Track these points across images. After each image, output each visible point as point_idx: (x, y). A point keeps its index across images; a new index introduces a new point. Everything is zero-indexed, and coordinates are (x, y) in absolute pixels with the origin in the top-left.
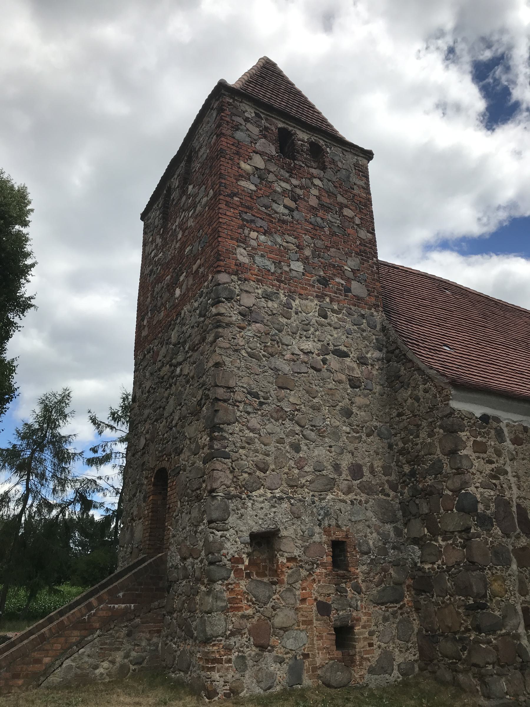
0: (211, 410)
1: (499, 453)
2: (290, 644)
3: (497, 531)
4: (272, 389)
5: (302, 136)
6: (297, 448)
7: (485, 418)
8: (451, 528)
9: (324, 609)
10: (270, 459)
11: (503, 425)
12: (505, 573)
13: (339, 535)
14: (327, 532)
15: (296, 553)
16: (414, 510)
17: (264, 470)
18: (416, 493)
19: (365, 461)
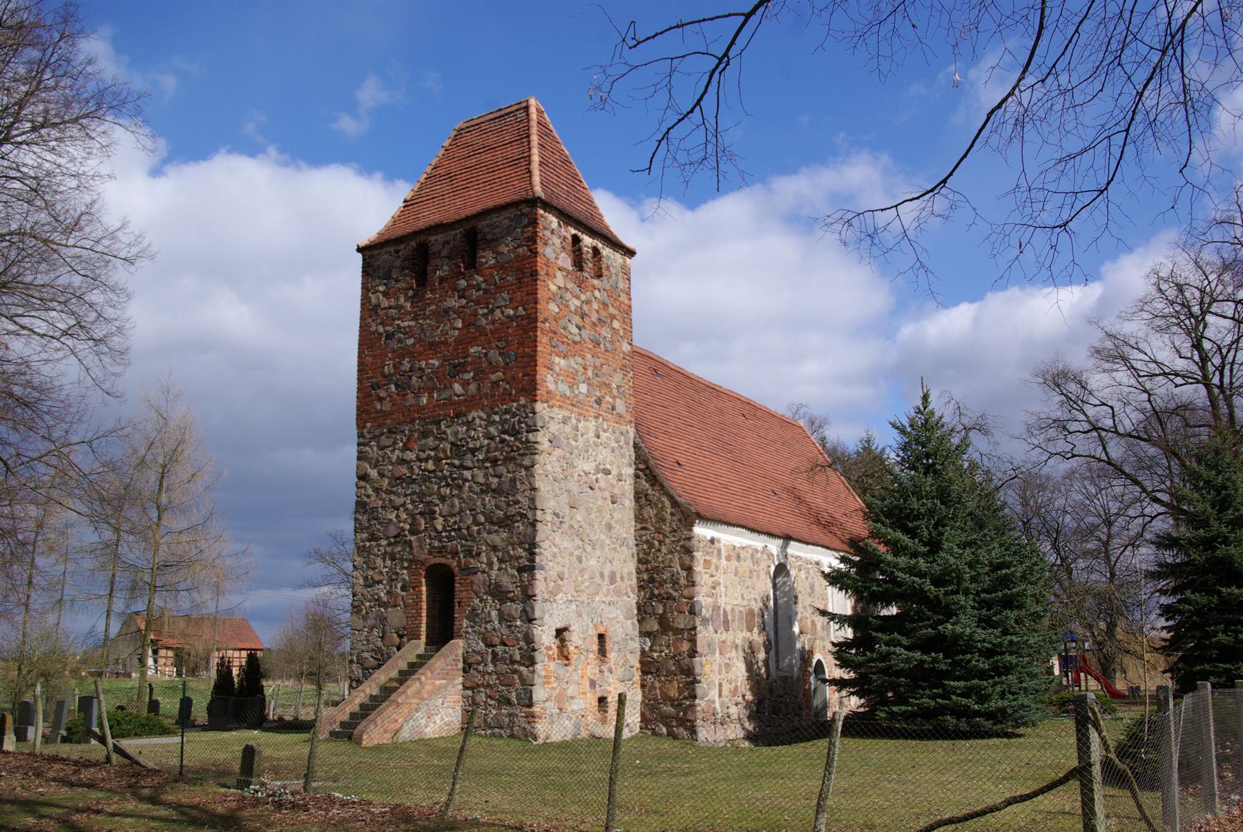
0: (1079, 749)
1: (717, 568)
2: (575, 707)
3: (711, 628)
4: (567, 510)
5: (587, 241)
6: (580, 560)
7: (712, 541)
8: (682, 626)
9: (593, 684)
10: (566, 570)
11: (721, 545)
12: (21, 736)
13: (601, 630)
14: (595, 627)
15: (580, 642)
16: (650, 610)
17: (562, 579)
18: (652, 596)
19: (616, 566)
